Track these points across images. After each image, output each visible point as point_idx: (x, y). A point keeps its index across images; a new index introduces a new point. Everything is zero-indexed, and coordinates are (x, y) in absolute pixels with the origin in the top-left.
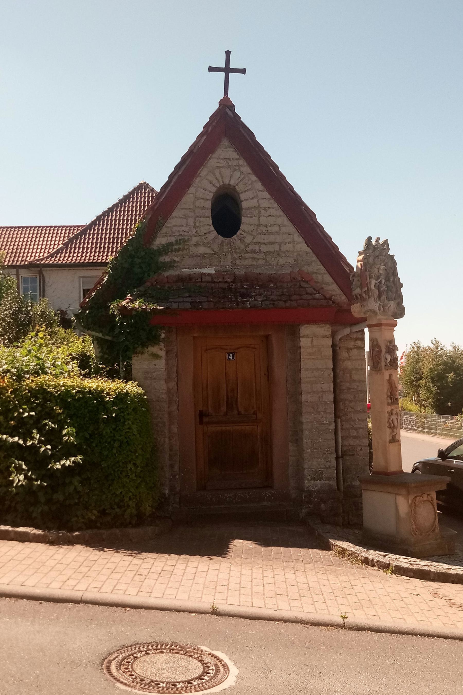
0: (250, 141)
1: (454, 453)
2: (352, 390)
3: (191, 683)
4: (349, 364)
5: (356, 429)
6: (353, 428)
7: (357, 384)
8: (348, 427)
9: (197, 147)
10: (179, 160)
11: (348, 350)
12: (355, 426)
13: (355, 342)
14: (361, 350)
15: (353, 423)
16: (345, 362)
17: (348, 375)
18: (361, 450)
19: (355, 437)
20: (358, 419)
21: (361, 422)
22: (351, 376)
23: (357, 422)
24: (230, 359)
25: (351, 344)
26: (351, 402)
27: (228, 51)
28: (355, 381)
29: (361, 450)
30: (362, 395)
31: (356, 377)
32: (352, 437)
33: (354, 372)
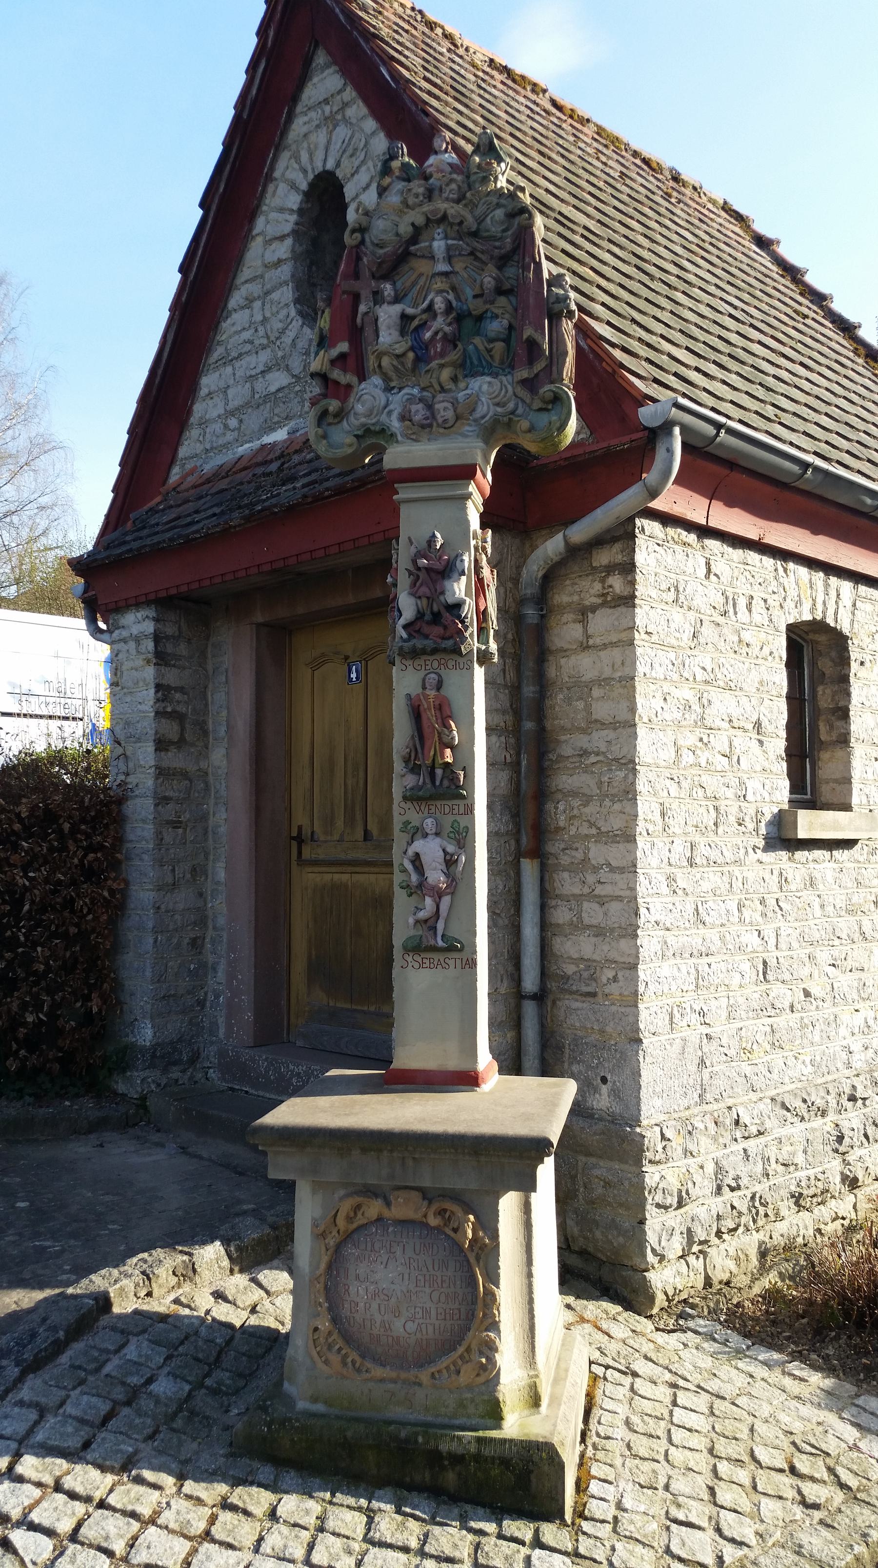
0: (341, 17)
1: (183, 487)
2: (593, 759)
3: (862, 1315)
4: (584, 665)
5: (602, 901)
6: (592, 896)
7: (609, 734)
8: (577, 891)
9: (248, 102)
10: (220, 148)
11: (584, 613)
12: (599, 890)
13: (603, 581)
14: (622, 609)
15: (591, 879)
16: (573, 660)
17: (580, 705)
18: (615, 979)
19: (600, 932)
20: (609, 865)
21: (617, 877)
22: (588, 709)
23: (604, 875)
24: (351, 679)
25: (589, 590)
26: (587, 800)
27: (818, 627)
28: (603, 725)
29: (615, 979)
30: (621, 774)
31: (602, 710)
32: (589, 927)
33: (596, 692)
